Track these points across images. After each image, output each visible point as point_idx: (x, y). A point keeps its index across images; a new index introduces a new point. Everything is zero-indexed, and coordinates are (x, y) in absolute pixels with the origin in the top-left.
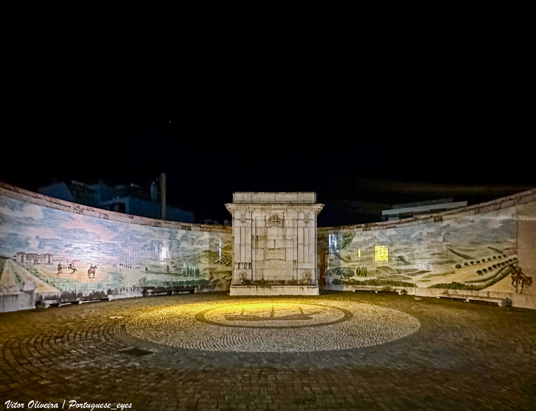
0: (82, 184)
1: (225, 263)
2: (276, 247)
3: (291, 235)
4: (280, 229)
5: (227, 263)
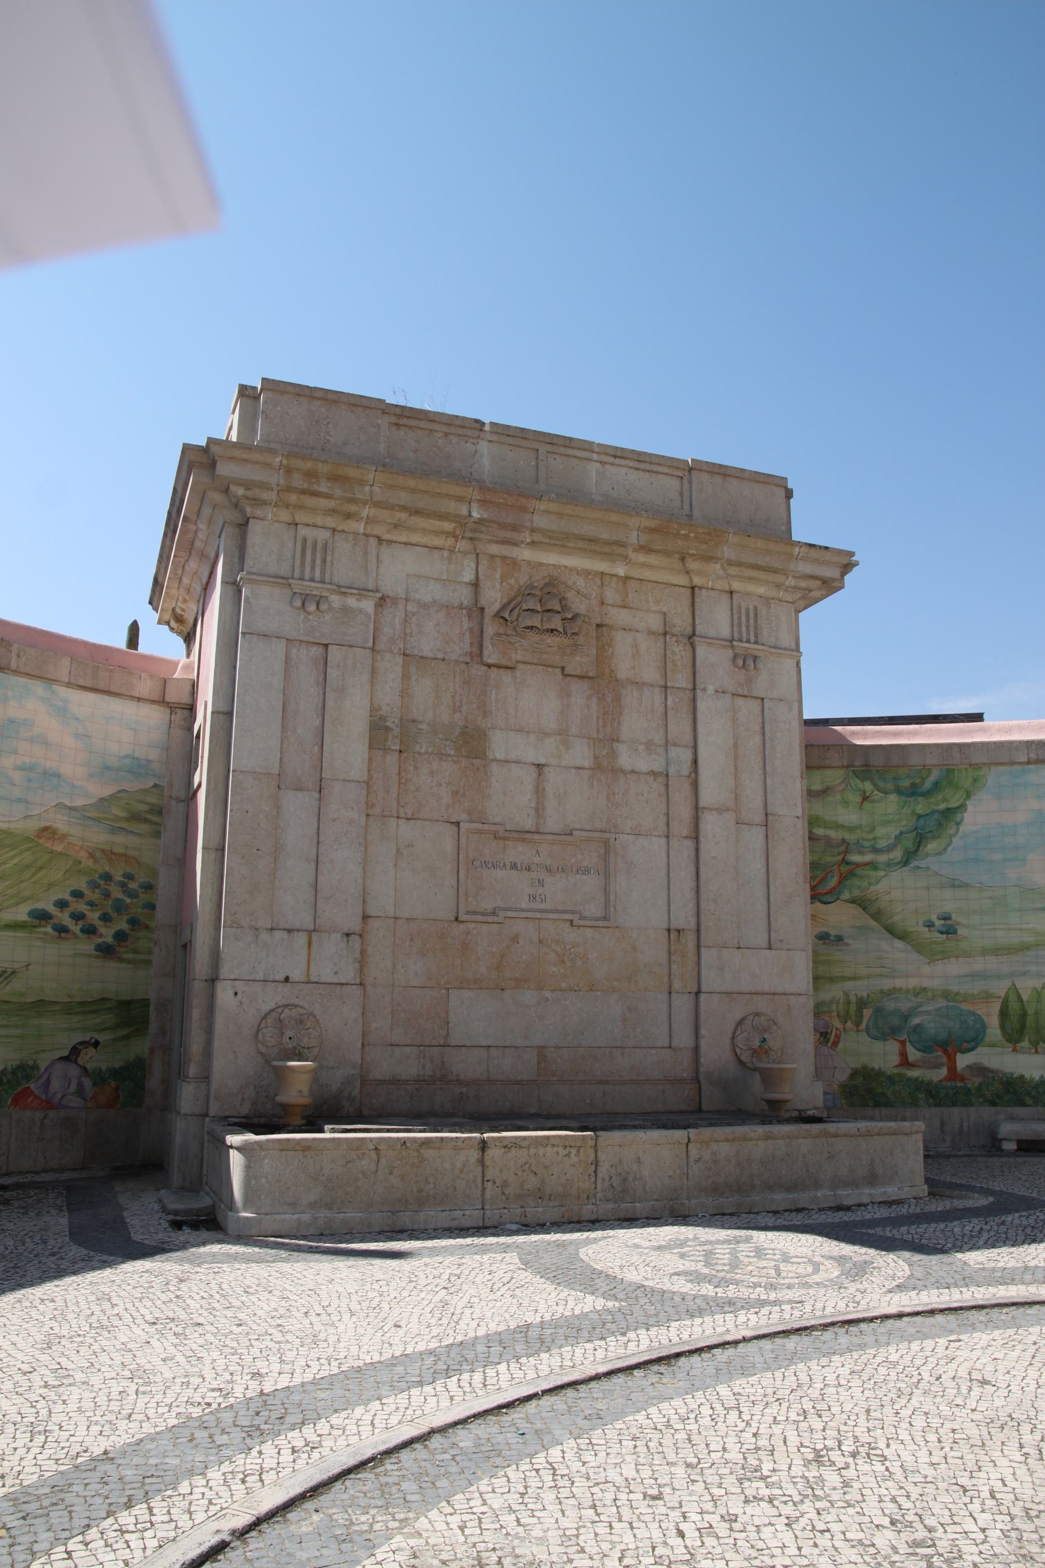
0: (477, 1135)
1: (90, 931)
2: (552, 823)
3: (649, 745)
4: (579, 691)
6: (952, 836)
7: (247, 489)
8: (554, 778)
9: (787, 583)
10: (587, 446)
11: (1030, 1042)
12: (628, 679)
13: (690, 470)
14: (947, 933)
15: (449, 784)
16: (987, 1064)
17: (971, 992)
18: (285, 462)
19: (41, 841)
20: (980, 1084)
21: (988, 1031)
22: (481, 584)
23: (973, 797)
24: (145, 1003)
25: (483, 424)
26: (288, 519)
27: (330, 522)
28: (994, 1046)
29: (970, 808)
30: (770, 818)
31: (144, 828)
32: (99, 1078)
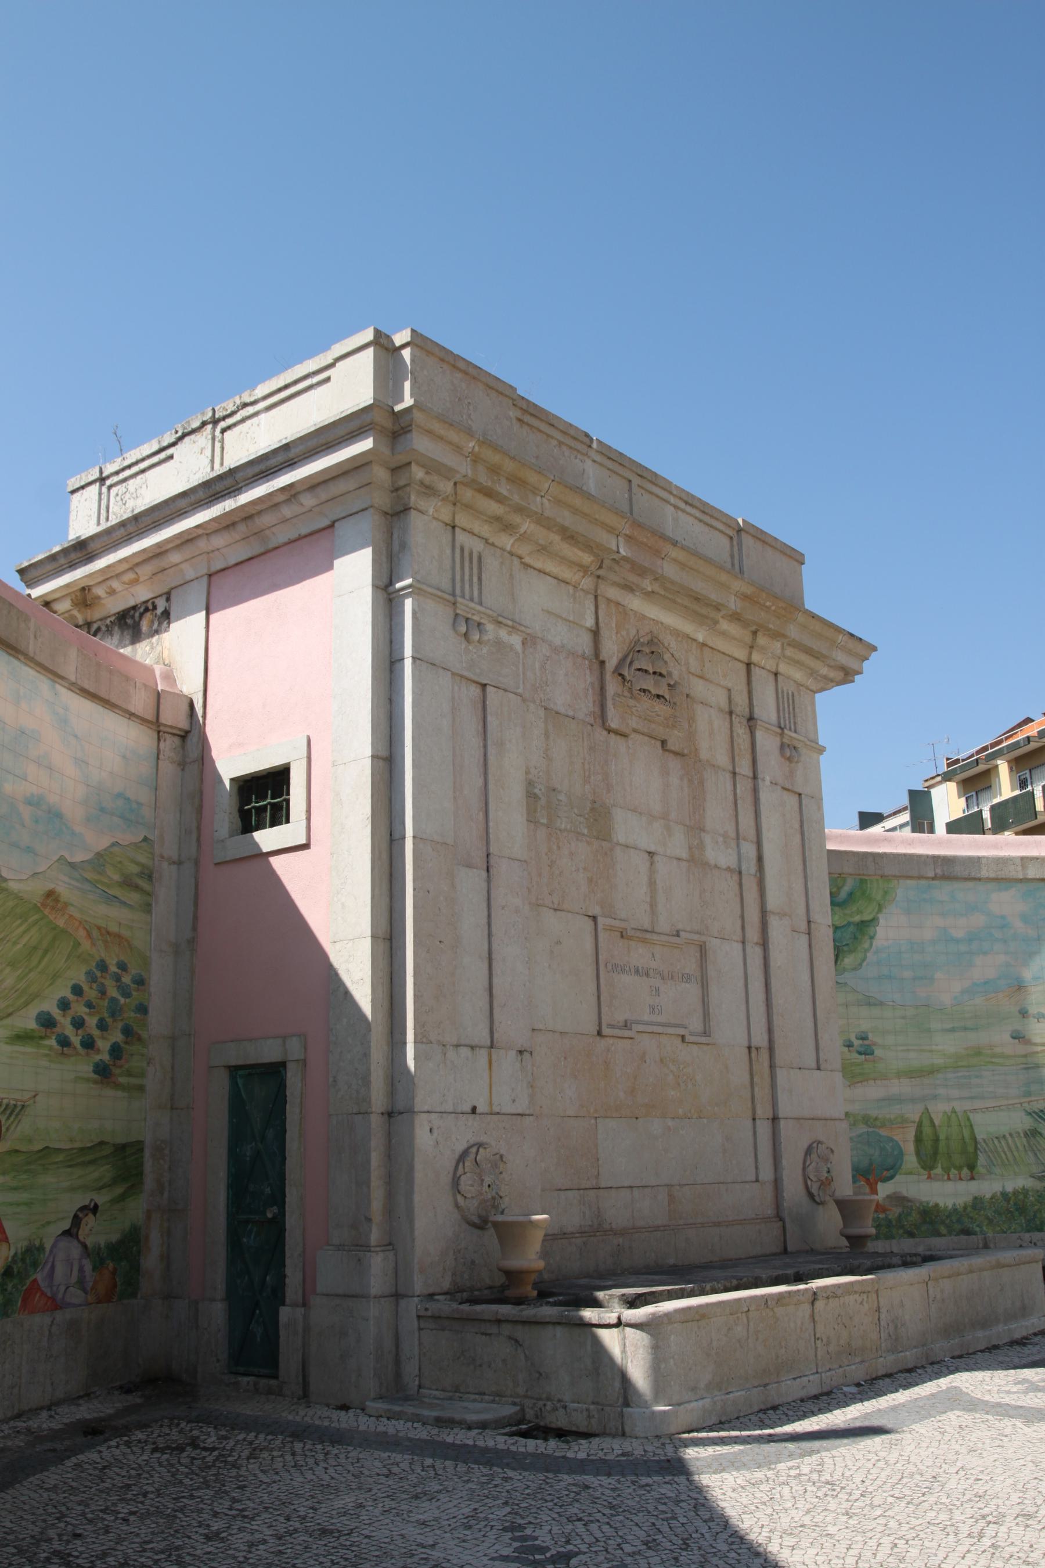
2: (663, 925)
4: (674, 764)
5: (104, 1045)
6: (866, 951)
7: (427, 473)
8: (662, 867)
9: (821, 672)
10: (666, 486)
11: (942, 1168)
12: (708, 761)
13: (740, 530)
14: (865, 1054)
15: (585, 869)
16: (905, 1193)
17: (888, 1116)
18: (477, 449)
19: (47, 911)
20: (900, 1215)
21: (906, 1158)
22: (602, 632)
23: (884, 911)
24: (138, 1147)
25: (591, 440)
26: (447, 518)
27: (485, 530)
28: (911, 1173)
29: (882, 922)
30: (813, 925)
31: (134, 897)
32: (97, 1256)
